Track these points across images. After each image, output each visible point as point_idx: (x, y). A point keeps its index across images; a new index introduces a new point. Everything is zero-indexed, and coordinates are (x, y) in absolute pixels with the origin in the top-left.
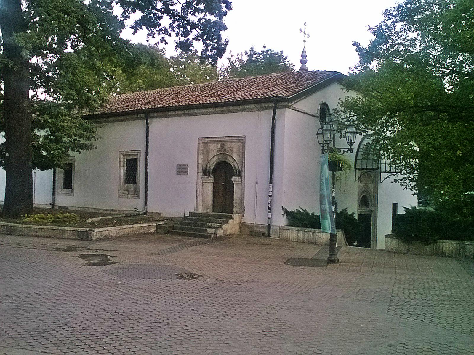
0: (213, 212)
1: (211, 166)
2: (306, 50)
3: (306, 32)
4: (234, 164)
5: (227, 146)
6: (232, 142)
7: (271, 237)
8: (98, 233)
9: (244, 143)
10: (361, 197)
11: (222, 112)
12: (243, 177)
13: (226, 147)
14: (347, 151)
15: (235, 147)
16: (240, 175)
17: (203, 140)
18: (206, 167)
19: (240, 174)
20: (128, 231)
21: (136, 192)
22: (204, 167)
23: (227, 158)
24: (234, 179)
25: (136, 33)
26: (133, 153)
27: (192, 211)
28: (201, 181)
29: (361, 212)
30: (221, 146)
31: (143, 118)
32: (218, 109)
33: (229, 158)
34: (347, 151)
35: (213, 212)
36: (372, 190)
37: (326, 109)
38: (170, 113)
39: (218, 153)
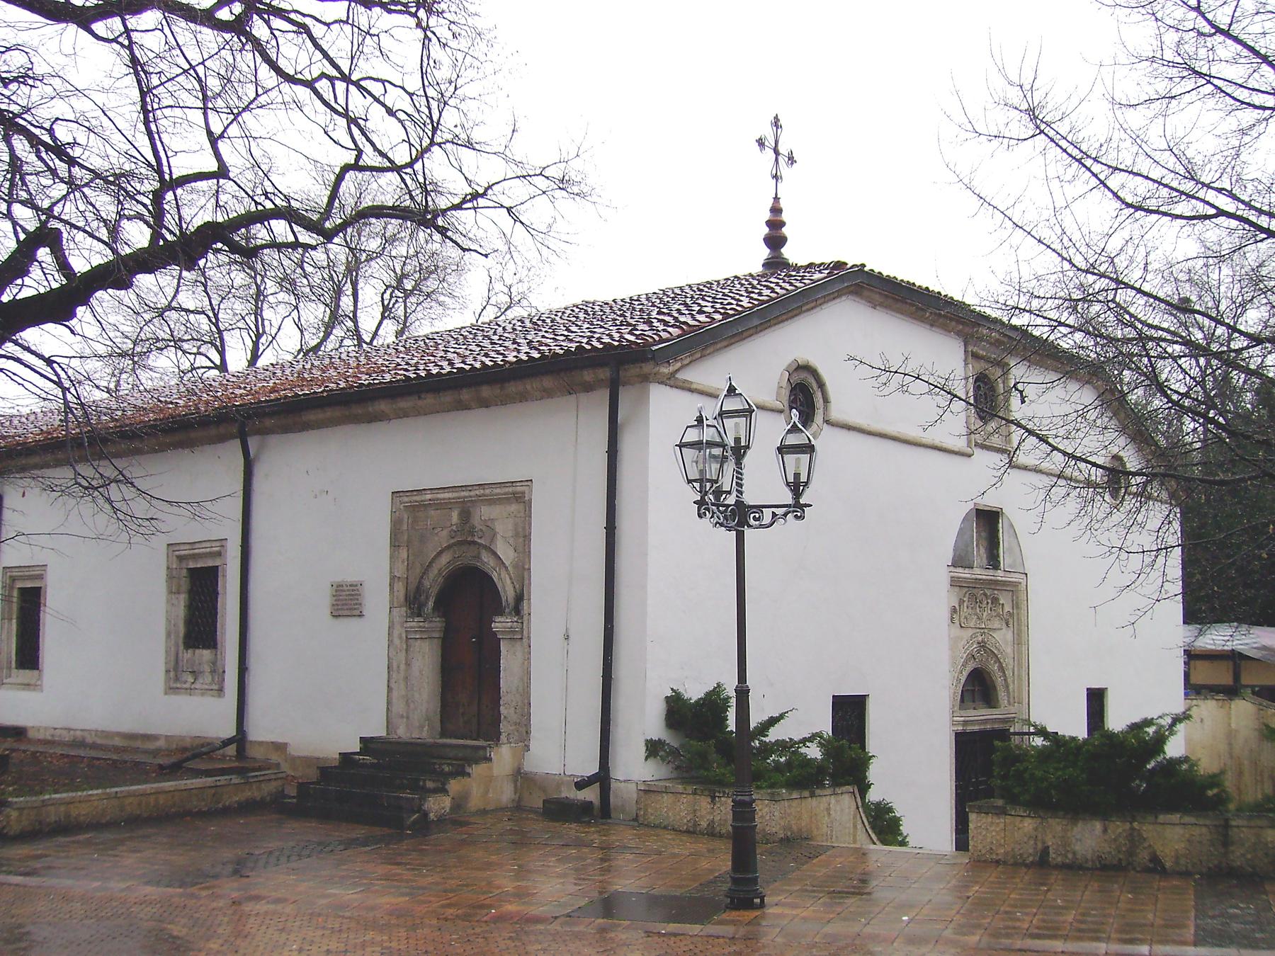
0: (444, 734)
1: (433, 582)
2: (783, 204)
3: (782, 149)
4: (499, 575)
5: (484, 512)
6: (491, 501)
7: (610, 818)
8: (25, 812)
9: (528, 505)
10: (965, 674)
11: (461, 406)
12: (525, 618)
13: (476, 521)
14: (785, 515)
15: (500, 519)
16: (517, 610)
17: (406, 499)
18: (420, 582)
19: (518, 605)
20: (140, 804)
21: (218, 672)
22: (412, 587)
23: (478, 557)
24: (500, 624)
25: (927, 288)
26: (208, 550)
27: (378, 730)
28: (404, 636)
29: (965, 723)
30: (460, 514)
31: (232, 437)
32: (447, 398)
33: (485, 557)
34: (785, 515)
35: (444, 734)
36: (1009, 650)
37: (815, 385)
38: (312, 416)
39: (452, 541)
